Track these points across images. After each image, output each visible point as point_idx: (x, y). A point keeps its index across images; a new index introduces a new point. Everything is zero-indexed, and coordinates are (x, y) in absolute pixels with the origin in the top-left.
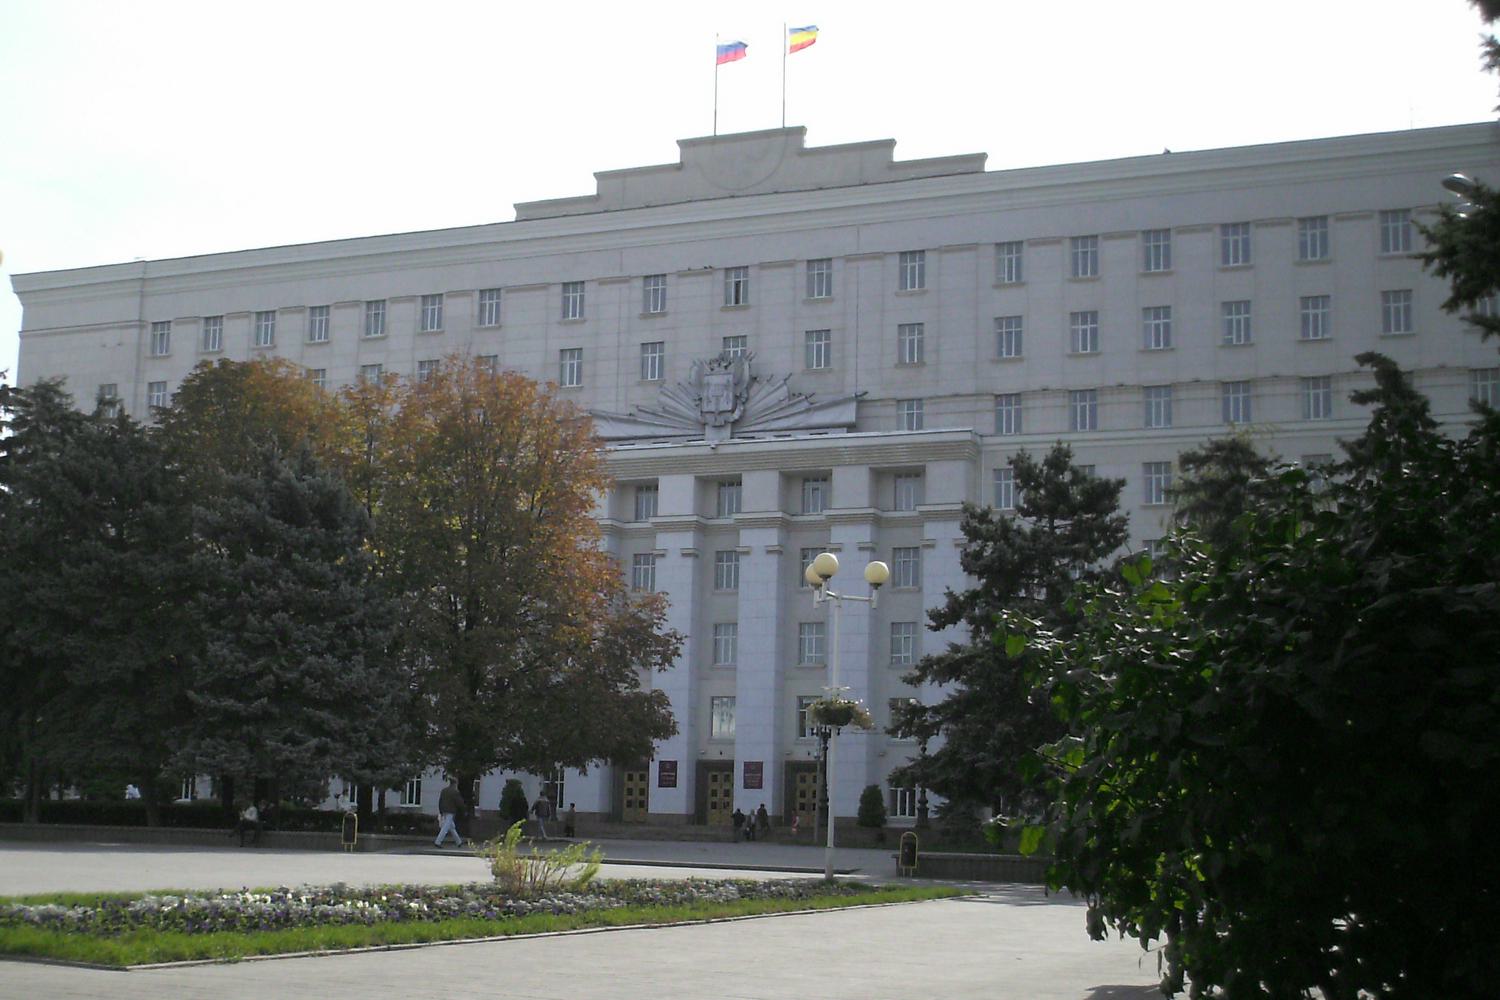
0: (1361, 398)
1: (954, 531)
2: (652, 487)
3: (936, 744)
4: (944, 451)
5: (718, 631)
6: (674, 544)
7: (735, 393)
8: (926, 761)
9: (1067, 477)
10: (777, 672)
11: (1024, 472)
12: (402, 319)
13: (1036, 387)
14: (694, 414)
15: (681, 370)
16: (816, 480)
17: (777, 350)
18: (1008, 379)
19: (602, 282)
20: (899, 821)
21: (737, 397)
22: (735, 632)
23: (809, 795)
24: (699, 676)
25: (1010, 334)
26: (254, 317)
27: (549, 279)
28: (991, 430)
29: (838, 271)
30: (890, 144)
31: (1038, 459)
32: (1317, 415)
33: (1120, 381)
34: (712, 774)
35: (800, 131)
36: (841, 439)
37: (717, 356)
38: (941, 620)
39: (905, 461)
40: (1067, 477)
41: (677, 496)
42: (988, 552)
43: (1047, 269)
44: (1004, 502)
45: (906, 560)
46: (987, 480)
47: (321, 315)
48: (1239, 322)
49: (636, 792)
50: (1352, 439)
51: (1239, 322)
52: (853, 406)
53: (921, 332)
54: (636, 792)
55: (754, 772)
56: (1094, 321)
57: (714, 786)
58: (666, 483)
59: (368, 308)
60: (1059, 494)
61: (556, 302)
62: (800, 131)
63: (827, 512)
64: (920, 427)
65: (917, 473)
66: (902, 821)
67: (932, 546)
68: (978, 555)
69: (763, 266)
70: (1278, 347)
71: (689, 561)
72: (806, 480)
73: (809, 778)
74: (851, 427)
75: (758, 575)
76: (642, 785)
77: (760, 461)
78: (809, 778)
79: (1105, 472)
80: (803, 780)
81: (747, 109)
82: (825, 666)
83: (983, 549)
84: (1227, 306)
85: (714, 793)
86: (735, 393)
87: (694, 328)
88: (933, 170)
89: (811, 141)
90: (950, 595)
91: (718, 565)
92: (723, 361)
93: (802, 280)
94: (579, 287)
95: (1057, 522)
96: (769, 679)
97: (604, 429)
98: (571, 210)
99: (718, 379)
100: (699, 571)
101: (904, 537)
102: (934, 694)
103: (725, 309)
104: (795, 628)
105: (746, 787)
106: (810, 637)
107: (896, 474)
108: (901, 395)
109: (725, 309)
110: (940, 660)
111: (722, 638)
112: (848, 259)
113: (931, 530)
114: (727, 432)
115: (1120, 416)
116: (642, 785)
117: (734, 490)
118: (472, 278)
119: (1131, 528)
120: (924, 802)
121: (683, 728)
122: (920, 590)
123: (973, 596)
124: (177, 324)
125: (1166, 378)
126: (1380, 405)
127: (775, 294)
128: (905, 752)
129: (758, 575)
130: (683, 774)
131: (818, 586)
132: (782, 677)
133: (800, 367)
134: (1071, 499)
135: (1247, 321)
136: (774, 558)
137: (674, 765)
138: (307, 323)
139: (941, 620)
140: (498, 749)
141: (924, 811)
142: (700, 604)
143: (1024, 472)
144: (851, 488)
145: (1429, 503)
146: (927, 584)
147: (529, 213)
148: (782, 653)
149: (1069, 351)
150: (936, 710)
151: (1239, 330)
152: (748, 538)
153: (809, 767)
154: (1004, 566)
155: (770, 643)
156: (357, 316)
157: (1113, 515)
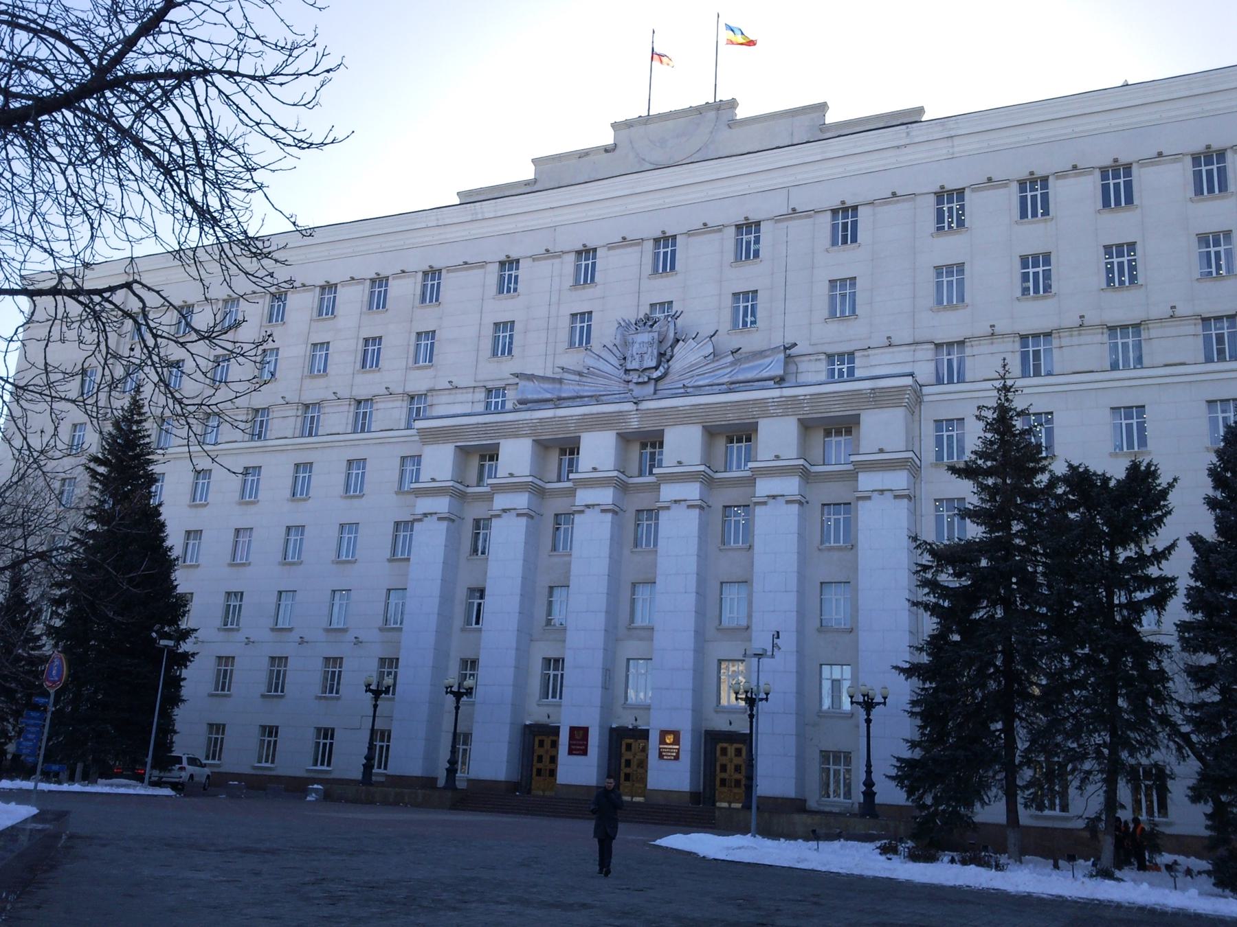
4: (878, 398)
10: (696, 632)
15: (604, 332)
21: (661, 355)
23: (731, 768)
30: (822, 107)
35: (733, 104)
39: (838, 411)
43: (992, 214)
47: (666, 246)
49: (546, 759)
54: (546, 759)
57: (724, 760)
62: (733, 104)
63: (750, 465)
78: (731, 750)
87: (621, 293)
89: (741, 113)
92: (647, 322)
93: (730, 244)
99: (645, 337)
100: (617, 528)
106: (731, 593)
108: (831, 350)
133: (725, 324)
135: (432, 344)
136: (795, 507)
138: (316, 300)
147: (470, 198)
153: (731, 737)
155: (690, 600)
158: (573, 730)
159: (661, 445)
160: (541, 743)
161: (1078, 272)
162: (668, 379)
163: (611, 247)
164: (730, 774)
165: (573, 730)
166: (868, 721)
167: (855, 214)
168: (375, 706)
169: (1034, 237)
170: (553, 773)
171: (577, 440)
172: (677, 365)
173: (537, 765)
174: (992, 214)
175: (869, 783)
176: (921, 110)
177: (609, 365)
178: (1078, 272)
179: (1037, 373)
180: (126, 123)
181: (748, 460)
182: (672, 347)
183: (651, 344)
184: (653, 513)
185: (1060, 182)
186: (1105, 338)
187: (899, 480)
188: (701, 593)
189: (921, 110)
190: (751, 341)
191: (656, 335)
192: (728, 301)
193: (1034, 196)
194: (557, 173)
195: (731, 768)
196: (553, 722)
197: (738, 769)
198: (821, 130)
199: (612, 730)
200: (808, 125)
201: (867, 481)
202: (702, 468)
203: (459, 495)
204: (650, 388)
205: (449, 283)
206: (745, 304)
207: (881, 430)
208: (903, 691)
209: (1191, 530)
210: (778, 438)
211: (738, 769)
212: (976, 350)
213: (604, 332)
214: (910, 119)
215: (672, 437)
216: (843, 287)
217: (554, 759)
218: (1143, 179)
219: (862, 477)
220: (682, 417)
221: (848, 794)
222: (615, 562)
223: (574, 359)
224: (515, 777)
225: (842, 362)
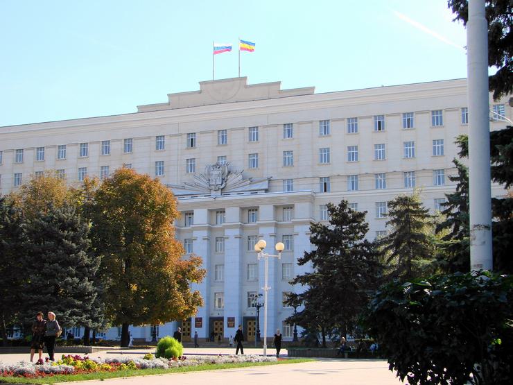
0: (453, 179)
1: (307, 228)
2: (191, 213)
3: (301, 308)
4: (301, 199)
5: (216, 268)
6: (201, 235)
7: (223, 177)
8: (297, 314)
9: (347, 211)
10: (240, 283)
11: (331, 209)
12: (29, 156)
13: (335, 174)
14: (207, 186)
15: (201, 168)
16: (253, 210)
17: (238, 160)
18: (325, 171)
19: (171, 136)
20: (286, 339)
21: (223, 179)
22: (223, 268)
23: (252, 329)
24: (210, 285)
25: (325, 155)
26: (36, 149)
27: (151, 135)
28: (319, 191)
29: (295, 127)
30: (279, 83)
31: (336, 204)
32: (439, 184)
33: (394, 170)
34: (215, 323)
35: (245, 78)
36: (262, 195)
37: (215, 164)
38: (302, 262)
39: (286, 202)
40: (347, 211)
41: (201, 217)
42: (318, 238)
43: (338, 130)
44: (326, 221)
45: (288, 240)
46: (317, 209)
47: (254, 130)
48: (438, 147)
49: (186, 329)
50: (449, 194)
51: (438, 147)
52: (267, 182)
53: (292, 154)
54: (186, 329)
55: (231, 320)
56: (442, 143)
57: (250, 326)
58: (196, 212)
59: (81, 146)
60: (345, 216)
61: (154, 144)
62: (245, 78)
63: (257, 222)
64: (292, 190)
65: (291, 207)
66: (288, 338)
67: (297, 235)
68: (315, 238)
69: (232, 130)
70: (424, 158)
71: (206, 241)
72: (251, 211)
73: (252, 323)
74: (266, 191)
75: (232, 247)
76: (188, 327)
77: (232, 203)
78: (252, 323)
79: (360, 210)
80: (250, 324)
81: (226, 69)
82: (258, 280)
83: (317, 236)
84: (406, 144)
85: (250, 329)
86: (223, 177)
87: (206, 153)
88: (288, 95)
89: (249, 82)
90: (305, 252)
91: (215, 241)
92: (217, 166)
93: (247, 135)
94: (162, 138)
95: (344, 227)
96: (237, 286)
97: (177, 192)
98: (160, 108)
99: (216, 172)
100: (210, 245)
101: (286, 231)
102: (300, 289)
103: (187, 149)
104: (266, 265)
105: (228, 327)
106: (252, 269)
107: (284, 208)
108: (284, 178)
109: (187, 149)
110: (302, 276)
111: (219, 270)
112: (264, 127)
113: (297, 229)
114: (220, 192)
115: (366, 184)
116: (221, 326)
117: (289, 211)
118: (123, 135)
119: (369, 227)
120: (296, 331)
121: (204, 302)
122: (293, 251)
123: (314, 253)
124: (69, 146)
125: (383, 170)
126: (459, 182)
127: (238, 140)
128: (289, 312)
129: (232, 247)
130: (205, 322)
131: (259, 252)
132: (241, 284)
133: (247, 168)
134: (347, 219)
135: (413, 149)
136: (238, 239)
137: (201, 319)
138: (36, 154)
139: (302, 262)
140: (52, 313)
141: (296, 334)
142: (210, 258)
143: (331, 209)
144: (266, 213)
145: (403, 219)
146: (296, 249)
147: (143, 109)
148: (241, 275)
149: (374, 159)
150: (301, 295)
151: (410, 153)
152: (228, 232)
153: (252, 318)
154: (325, 241)
155: (237, 272)
156: (55, 151)
157: (363, 223)
159: (193, 214)
161: (366, 153)
162: (226, 189)
167: (441, 113)
168: (258, 312)
169: (409, 135)
171: (259, 207)
172: (229, 183)
174: (338, 130)
176: (313, 88)
177: (204, 183)
178: (366, 153)
179: (357, 189)
182: (227, 176)
186: (346, 180)
188: (241, 269)
189: (313, 88)
193: (353, 126)
194: (178, 101)
195: (252, 329)
198: (279, 92)
199: (244, 318)
200: (271, 90)
203: (210, 229)
205: (135, 144)
206: (254, 161)
212: (362, 179)
213: (201, 168)
214: (308, 92)
216: (160, 164)
218: (361, 123)
222: (242, 256)
223: (188, 178)
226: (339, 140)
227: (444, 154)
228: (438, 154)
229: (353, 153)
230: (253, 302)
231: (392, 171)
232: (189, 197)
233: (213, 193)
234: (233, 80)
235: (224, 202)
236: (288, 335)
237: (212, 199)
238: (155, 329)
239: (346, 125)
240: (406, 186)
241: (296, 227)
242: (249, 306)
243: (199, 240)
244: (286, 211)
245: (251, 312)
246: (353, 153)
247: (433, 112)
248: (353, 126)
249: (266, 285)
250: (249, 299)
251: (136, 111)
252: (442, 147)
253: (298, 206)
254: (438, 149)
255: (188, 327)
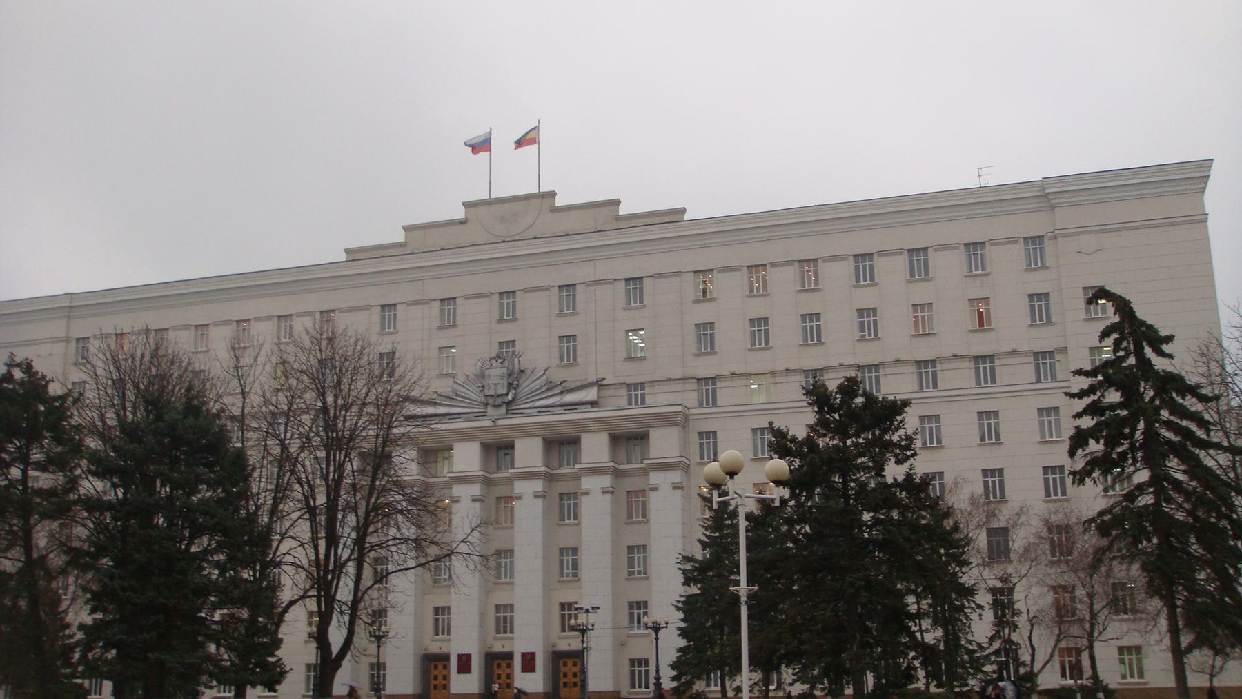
17: (538, 353)
21: (510, 385)
30: (617, 202)
35: (552, 195)
39: (634, 427)
49: (440, 678)
54: (440, 678)
62: (552, 195)
63: (577, 466)
67: (587, 494)
69: (527, 290)
70: (1012, 329)
74: (593, 404)
75: (529, 512)
77: (528, 431)
78: (570, 663)
84: (860, 312)
107: (628, 440)
117: (571, 448)
130: (476, 664)
147: (354, 255)
152: (519, 487)
158: (460, 657)
160: (436, 667)
163: (468, 297)
164: (570, 679)
165: (460, 657)
166: (657, 639)
170: (445, 687)
173: (563, 680)
175: (658, 678)
180: (341, 503)
181: (575, 463)
183: (502, 377)
184: (509, 499)
185: (774, 269)
187: (676, 476)
190: (572, 376)
191: (505, 370)
192: (556, 342)
193: (864, 265)
196: (444, 650)
197: (575, 675)
201: (655, 478)
202: (543, 469)
204: (503, 410)
207: (664, 444)
208: (676, 618)
209: (1176, 341)
210: (595, 449)
211: (575, 675)
214: (675, 216)
215: (520, 445)
217: (445, 678)
219: (652, 474)
220: (528, 431)
221: (647, 687)
224: (418, 691)
225: (636, 390)
226: (893, 288)
227: (717, 349)
228: (1041, 319)
229: (760, 328)
230: (573, 622)
231: (727, 372)
232: (557, 410)
233: (490, 410)
234: (527, 197)
235: (512, 427)
236: (640, 687)
237: (489, 423)
238: (379, 677)
239: (963, 257)
240: (1038, 381)
241: (652, 474)
242: (563, 630)
243: (665, 489)
244: (565, 449)
245: (571, 643)
246: (760, 328)
247: (910, 251)
248: (864, 265)
249: (743, 577)
250: (563, 616)
251: (343, 257)
252: (875, 322)
253: (656, 435)
254: (1040, 310)
255: (508, 671)
